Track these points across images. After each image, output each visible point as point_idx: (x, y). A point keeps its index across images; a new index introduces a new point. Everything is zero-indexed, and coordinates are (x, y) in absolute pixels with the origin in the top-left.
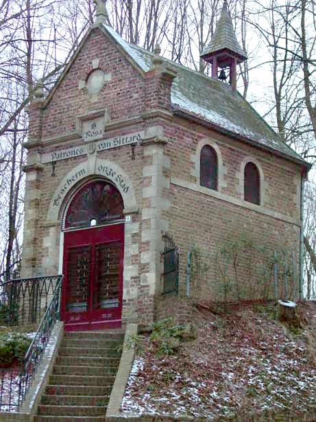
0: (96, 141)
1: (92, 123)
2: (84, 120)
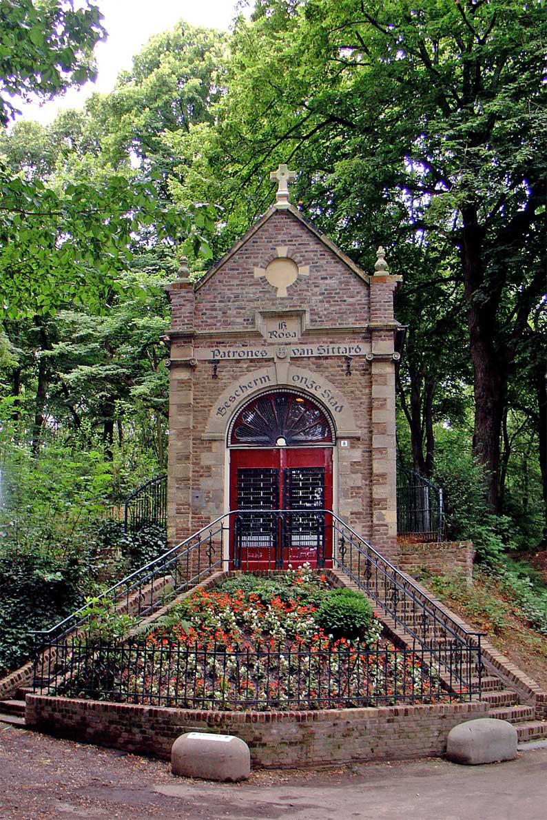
2: (80, 297)
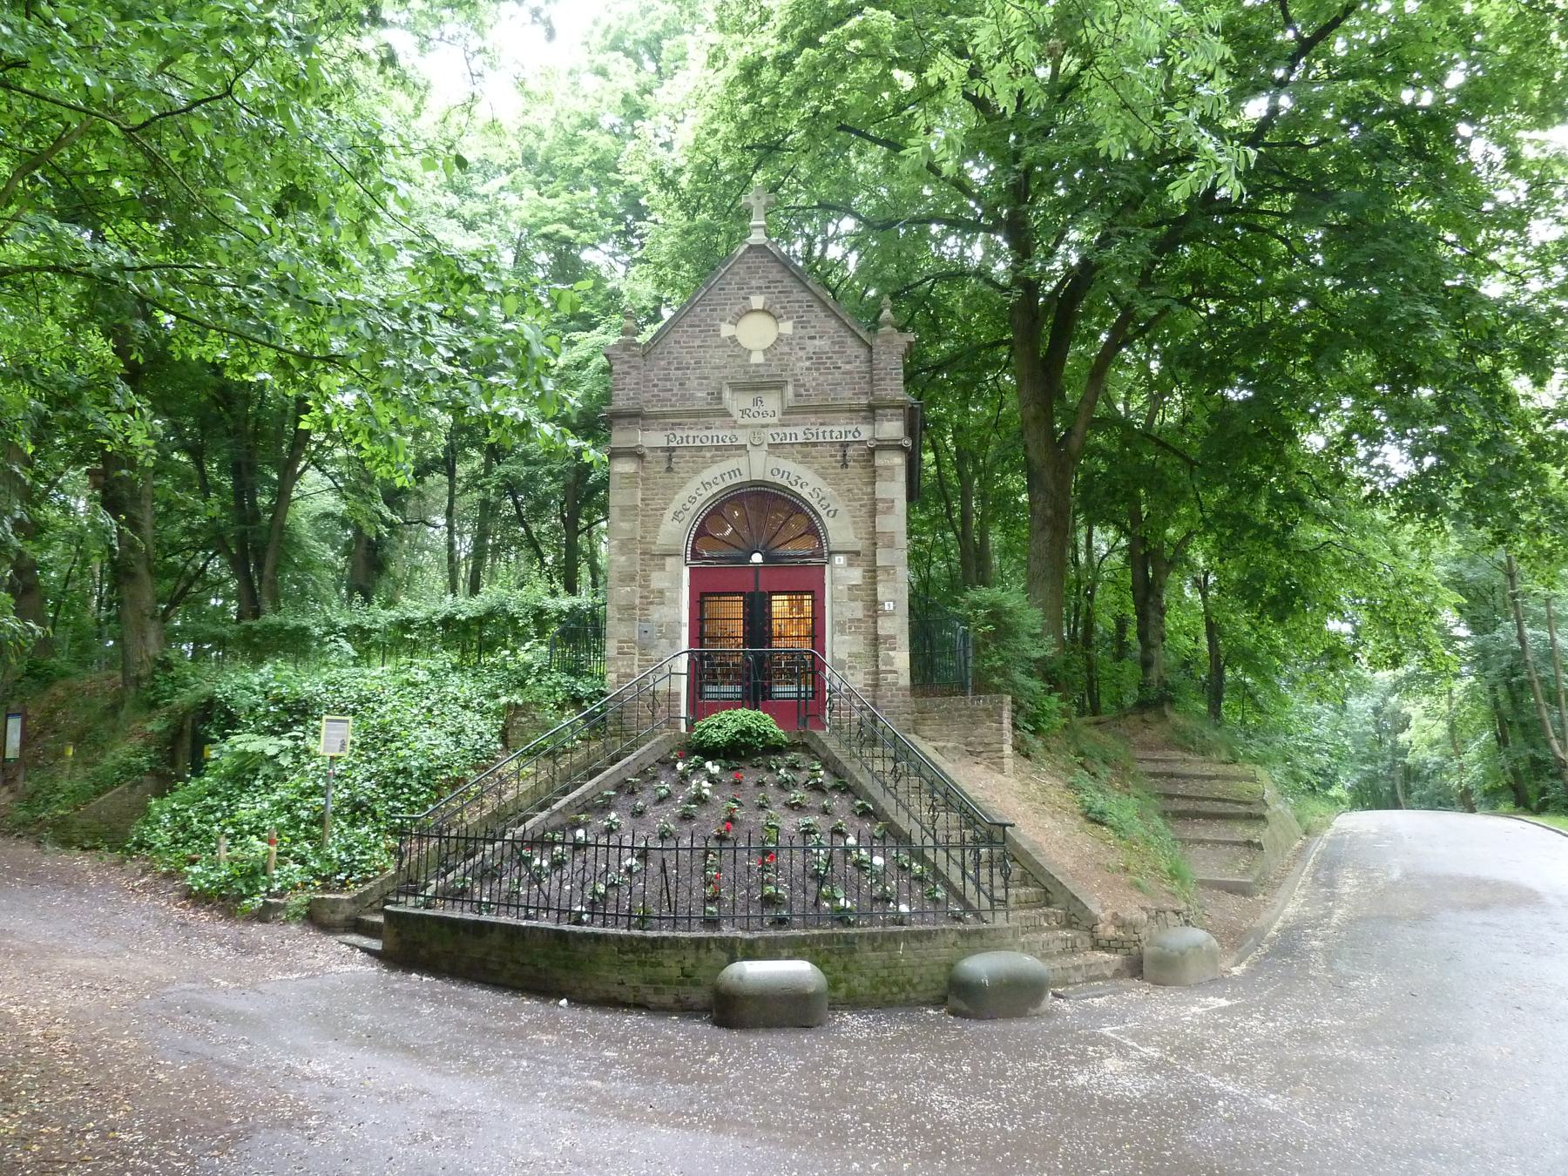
0: (767, 426)
1: (753, 395)
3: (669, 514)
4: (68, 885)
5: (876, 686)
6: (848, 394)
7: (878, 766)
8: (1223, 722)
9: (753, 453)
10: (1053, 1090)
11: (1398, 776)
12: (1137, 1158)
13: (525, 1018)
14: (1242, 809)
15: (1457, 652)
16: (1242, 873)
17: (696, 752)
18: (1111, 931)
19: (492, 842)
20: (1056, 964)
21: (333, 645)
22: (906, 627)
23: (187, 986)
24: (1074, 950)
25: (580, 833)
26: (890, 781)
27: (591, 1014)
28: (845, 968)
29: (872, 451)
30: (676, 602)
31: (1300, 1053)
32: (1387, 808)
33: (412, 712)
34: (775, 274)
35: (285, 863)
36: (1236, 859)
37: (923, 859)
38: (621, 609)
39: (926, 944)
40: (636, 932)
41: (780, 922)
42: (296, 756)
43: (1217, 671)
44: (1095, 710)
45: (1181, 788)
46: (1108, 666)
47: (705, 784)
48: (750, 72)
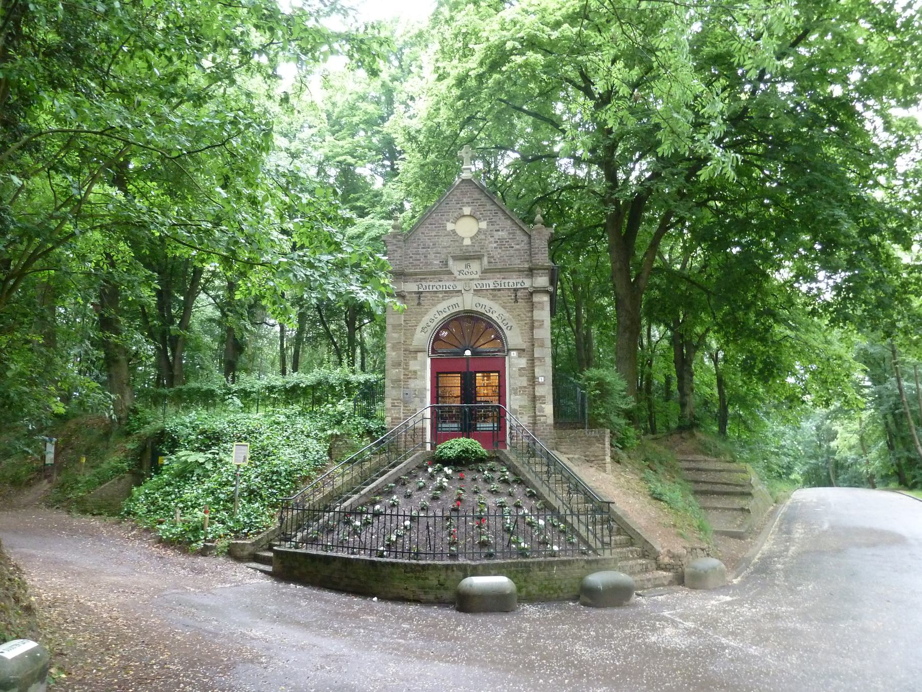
0: (472, 280)
3: (419, 329)
4: (92, 535)
5: (534, 424)
6: (518, 261)
7: (538, 468)
8: (728, 437)
9: (466, 295)
10: (639, 644)
11: (831, 466)
12: (684, 678)
13: (356, 607)
14: (739, 489)
15: (863, 396)
16: (739, 526)
17: (438, 462)
18: (667, 560)
19: (329, 512)
20: (638, 578)
21: (230, 401)
22: (551, 392)
23: (174, 591)
24: (646, 570)
25: (377, 507)
26: (545, 477)
27: (390, 606)
28: (525, 581)
29: (531, 294)
30: (424, 378)
31: (769, 625)
32: (825, 486)
33: (279, 440)
34: (476, 195)
35: (213, 524)
36: (735, 518)
37: (565, 522)
38: (393, 381)
39: (568, 567)
40: (414, 562)
41: (490, 556)
42: (215, 464)
43: (724, 408)
44: (653, 431)
45: (703, 477)
46: (661, 404)
47: (444, 480)
48: (461, 81)
